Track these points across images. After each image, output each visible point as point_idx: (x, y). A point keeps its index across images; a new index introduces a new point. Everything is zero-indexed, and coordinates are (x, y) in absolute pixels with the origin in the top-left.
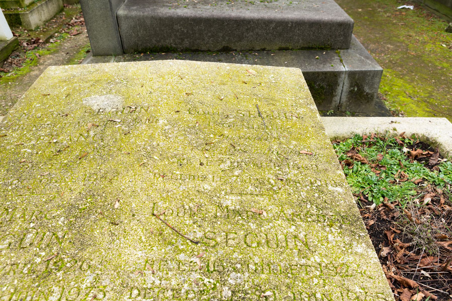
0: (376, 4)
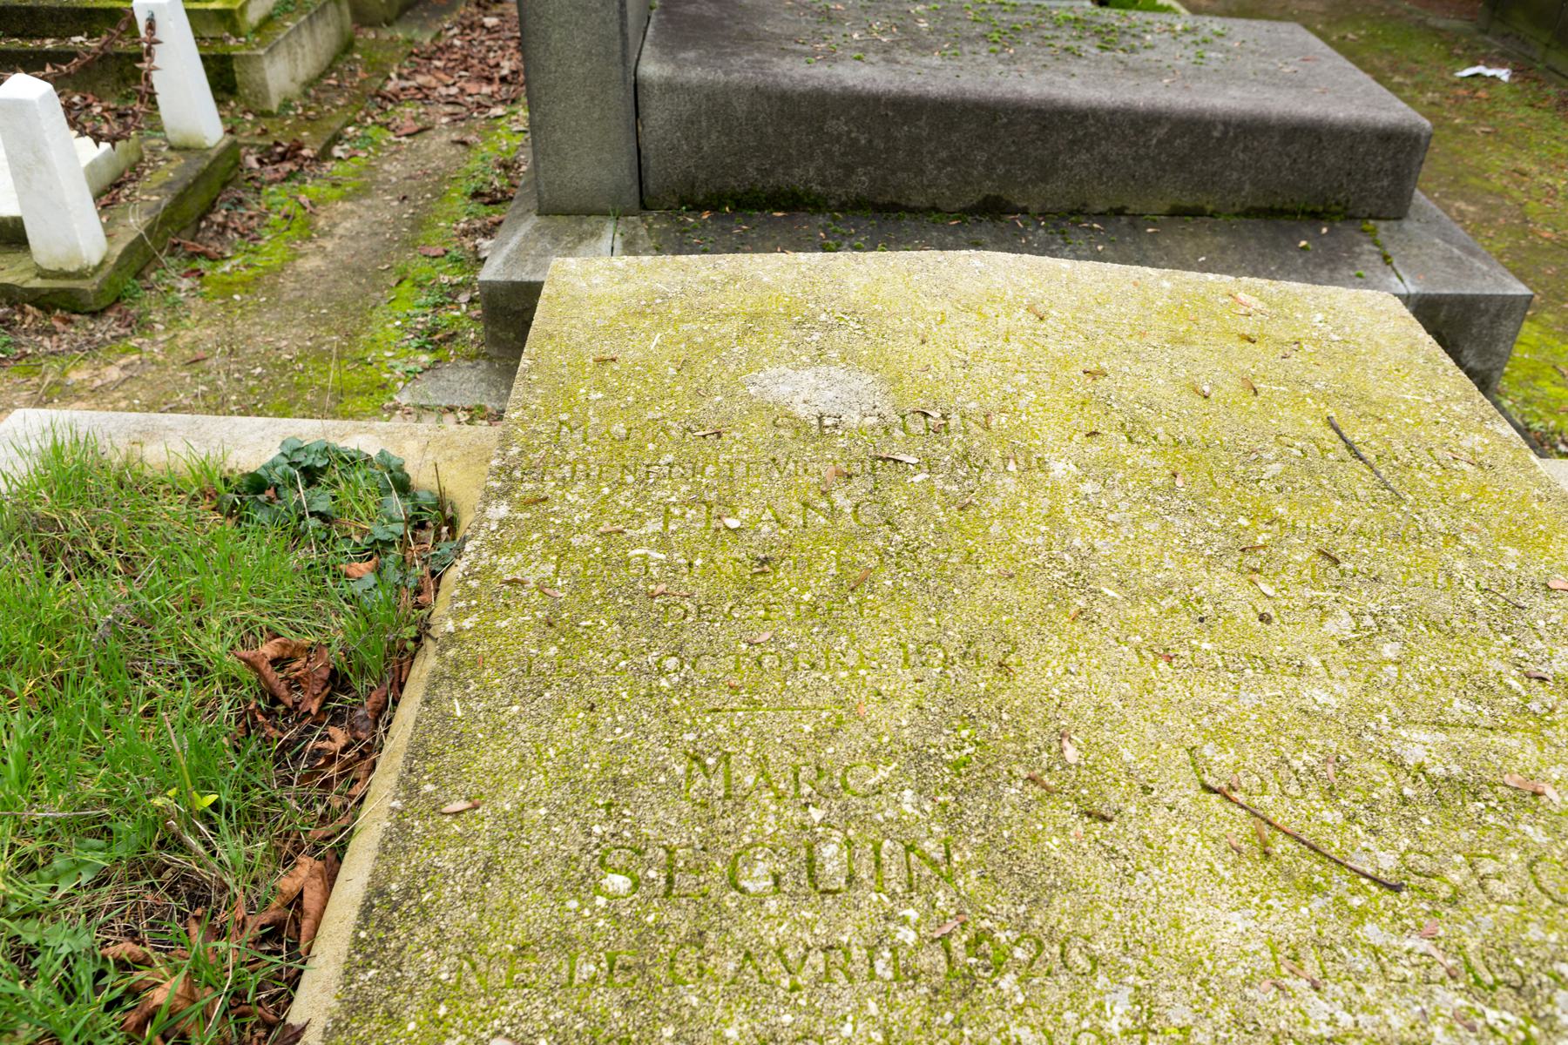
0: (1381, 58)
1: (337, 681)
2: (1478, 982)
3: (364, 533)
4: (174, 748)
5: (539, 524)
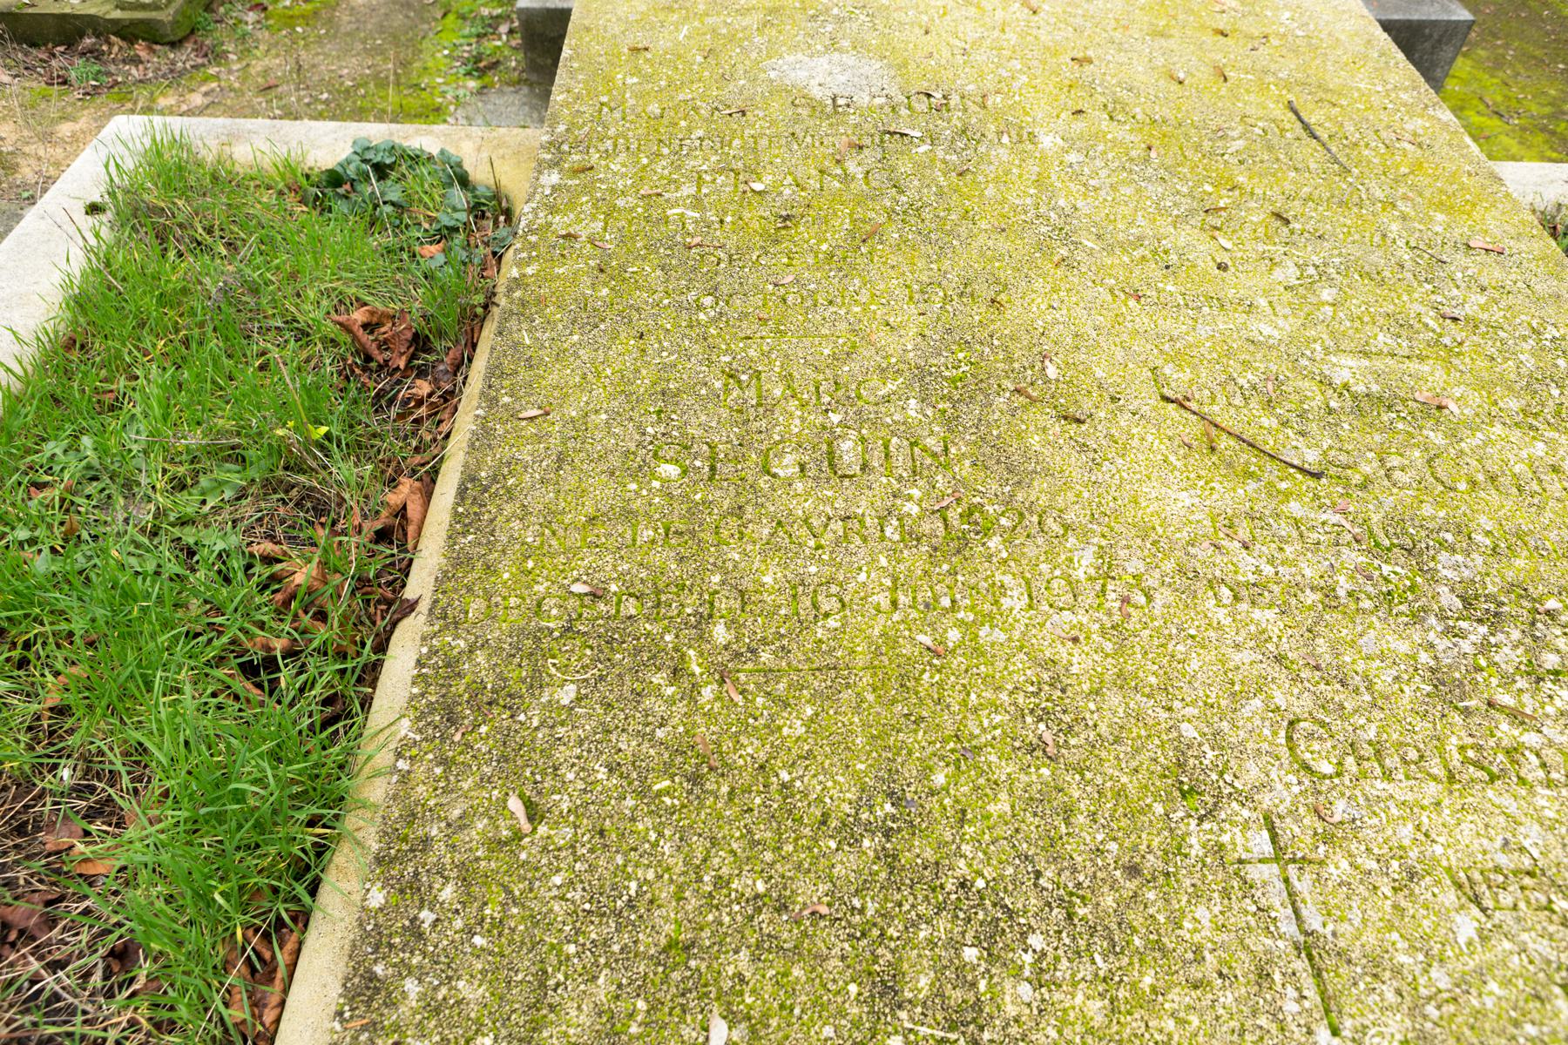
1: (420, 343)
2: (1377, 545)
3: (431, 220)
4: (287, 395)
5: (587, 189)
